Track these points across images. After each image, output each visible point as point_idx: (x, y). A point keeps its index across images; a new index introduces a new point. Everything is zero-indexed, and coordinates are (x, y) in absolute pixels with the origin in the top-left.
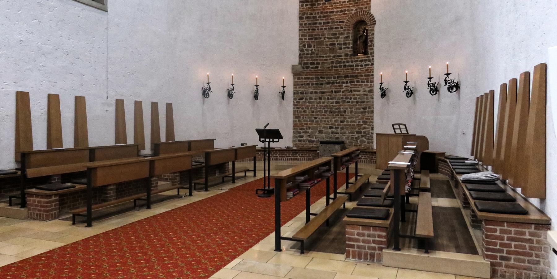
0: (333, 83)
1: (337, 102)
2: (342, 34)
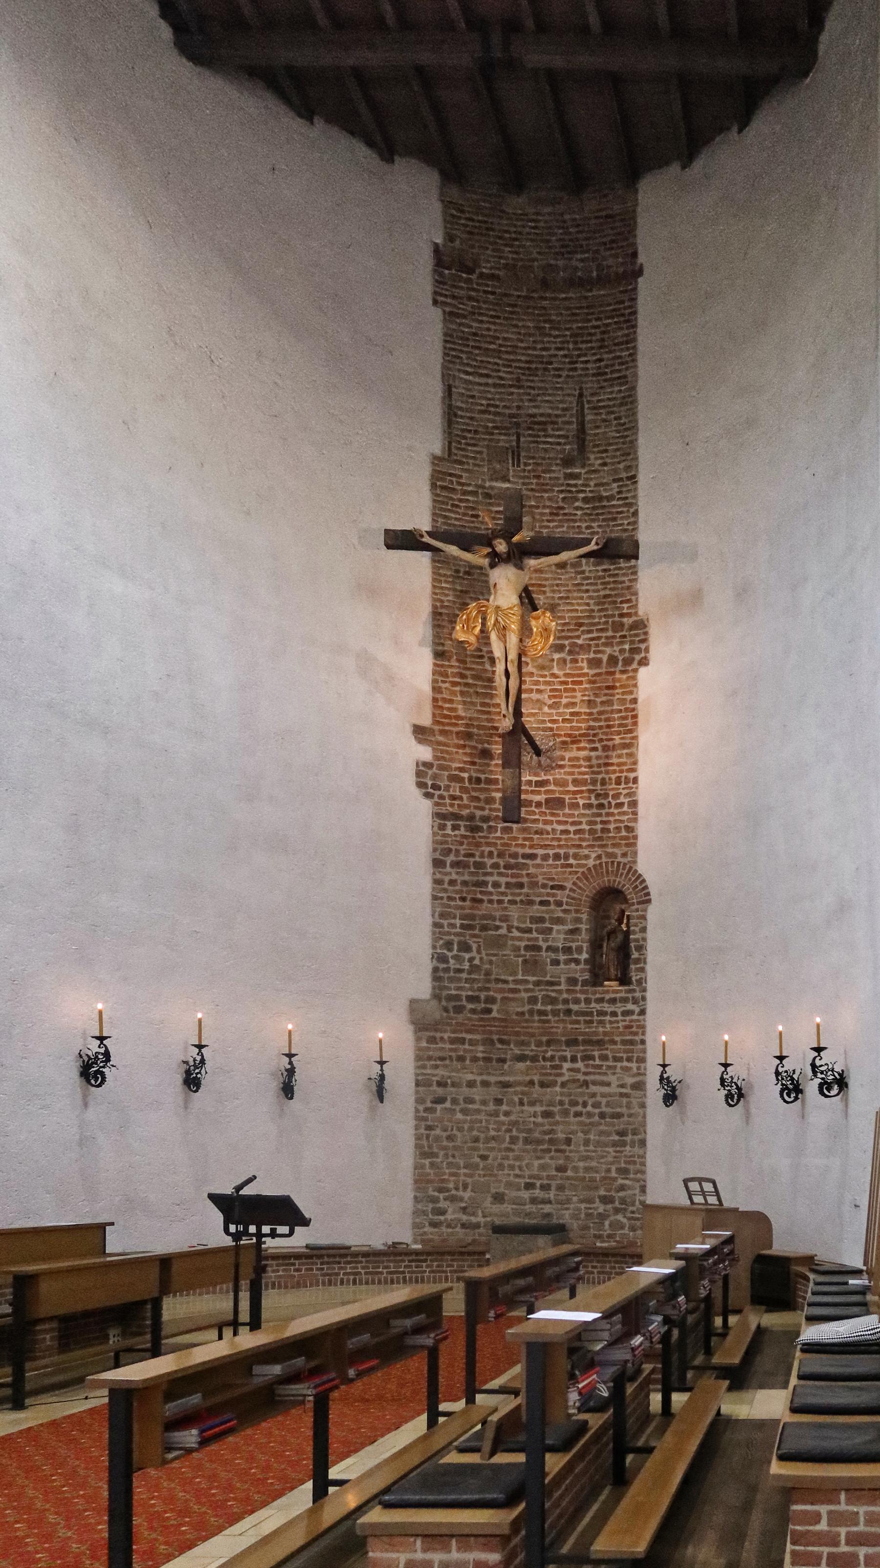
1: (547, 1114)
2: (559, 921)
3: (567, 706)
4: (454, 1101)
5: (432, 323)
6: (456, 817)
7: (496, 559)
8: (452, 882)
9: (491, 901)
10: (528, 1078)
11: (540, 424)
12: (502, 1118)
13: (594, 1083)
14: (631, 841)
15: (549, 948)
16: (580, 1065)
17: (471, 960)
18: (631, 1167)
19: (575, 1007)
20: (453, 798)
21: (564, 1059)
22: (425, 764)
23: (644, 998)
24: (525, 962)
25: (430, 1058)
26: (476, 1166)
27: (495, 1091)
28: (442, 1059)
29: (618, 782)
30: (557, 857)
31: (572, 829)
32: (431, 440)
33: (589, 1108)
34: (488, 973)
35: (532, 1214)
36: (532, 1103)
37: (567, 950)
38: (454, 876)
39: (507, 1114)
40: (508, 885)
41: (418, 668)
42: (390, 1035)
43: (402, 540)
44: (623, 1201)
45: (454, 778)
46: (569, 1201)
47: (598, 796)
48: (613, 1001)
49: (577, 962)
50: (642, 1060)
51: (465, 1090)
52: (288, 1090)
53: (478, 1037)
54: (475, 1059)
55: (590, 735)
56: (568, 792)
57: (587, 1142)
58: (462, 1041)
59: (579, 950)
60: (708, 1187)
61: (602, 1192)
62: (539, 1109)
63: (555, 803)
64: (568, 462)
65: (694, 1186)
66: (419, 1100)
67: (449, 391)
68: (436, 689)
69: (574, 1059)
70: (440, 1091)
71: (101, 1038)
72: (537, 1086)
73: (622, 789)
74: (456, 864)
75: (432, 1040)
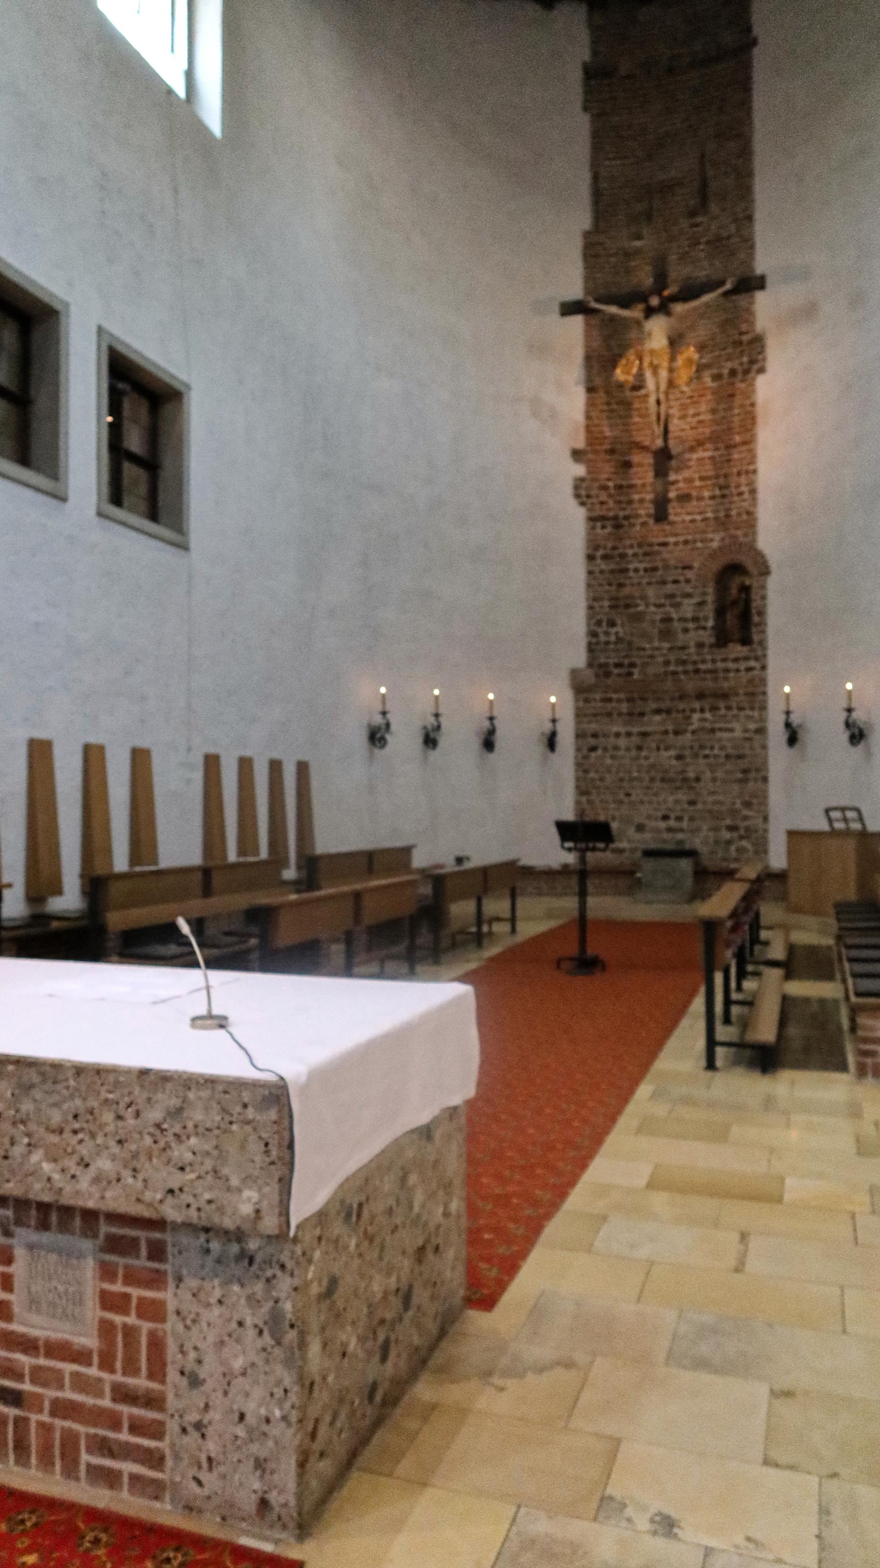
1: (679, 757)
2: (689, 596)
3: (694, 415)
4: (605, 749)
5: (580, 124)
6: (603, 518)
7: (650, 312)
8: (602, 572)
9: (632, 585)
10: (663, 728)
11: (667, 188)
12: (642, 761)
13: (720, 729)
14: (750, 521)
15: (681, 619)
16: (708, 715)
17: (617, 633)
18: (754, 801)
19: (702, 667)
20: (602, 503)
21: (693, 711)
22: (582, 480)
23: (765, 656)
24: (660, 632)
25: (585, 715)
26: (621, 802)
27: (635, 740)
28: (595, 715)
29: (739, 474)
30: (686, 542)
31: (698, 517)
32: (583, 220)
33: (716, 751)
34: (630, 644)
35: (669, 841)
36: (667, 749)
37: (695, 619)
38: (603, 567)
39: (647, 758)
40: (646, 570)
41: (572, 403)
42: (557, 699)
43: (569, 309)
44: (747, 829)
45: (605, 488)
46: (698, 829)
47: (721, 488)
48: (736, 660)
49: (704, 628)
50: (763, 708)
51: (612, 740)
52: (489, 744)
53: (622, 696)
54: (620, 714)
55: (714, 439)
56: (696, 487)
57: (714, 780)
58: (610, 700)
59: (706, 619)
60: (850, 814)
61: (728, 822)
62: (672, 753)
63: (684, 498)
64: (692, 214)
65: (835, 815)
66: (578, 750)
67: (596, 177)
68: (588, 417)
69: (702, 710)
70: (592, 741)
71: (384, 713)
72: (671, 735)
73: (743, 480)
74: (605, 557)
75: (587, 701)
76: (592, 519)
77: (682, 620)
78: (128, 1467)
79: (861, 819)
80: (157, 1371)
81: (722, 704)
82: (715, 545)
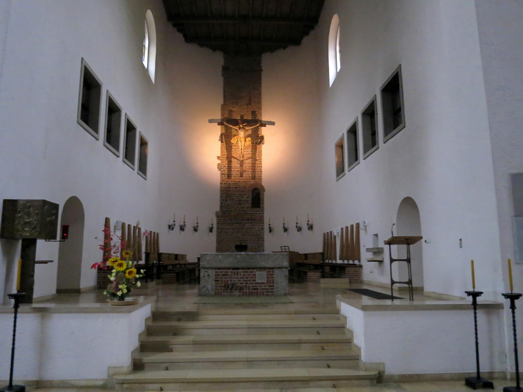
0: (240, 223)
1: (242, 235)
2: (245, 195)
5: (221, 79)
32: (221, 102)
50: (263, 223)
60: (286, 248)
66: (217, 232)
76: (222, 174)
77: (244, 200)
78: (270, 293)
79: (289, 249)
80: (273, 283)
81: (253, 222)
82: (252, 183)
